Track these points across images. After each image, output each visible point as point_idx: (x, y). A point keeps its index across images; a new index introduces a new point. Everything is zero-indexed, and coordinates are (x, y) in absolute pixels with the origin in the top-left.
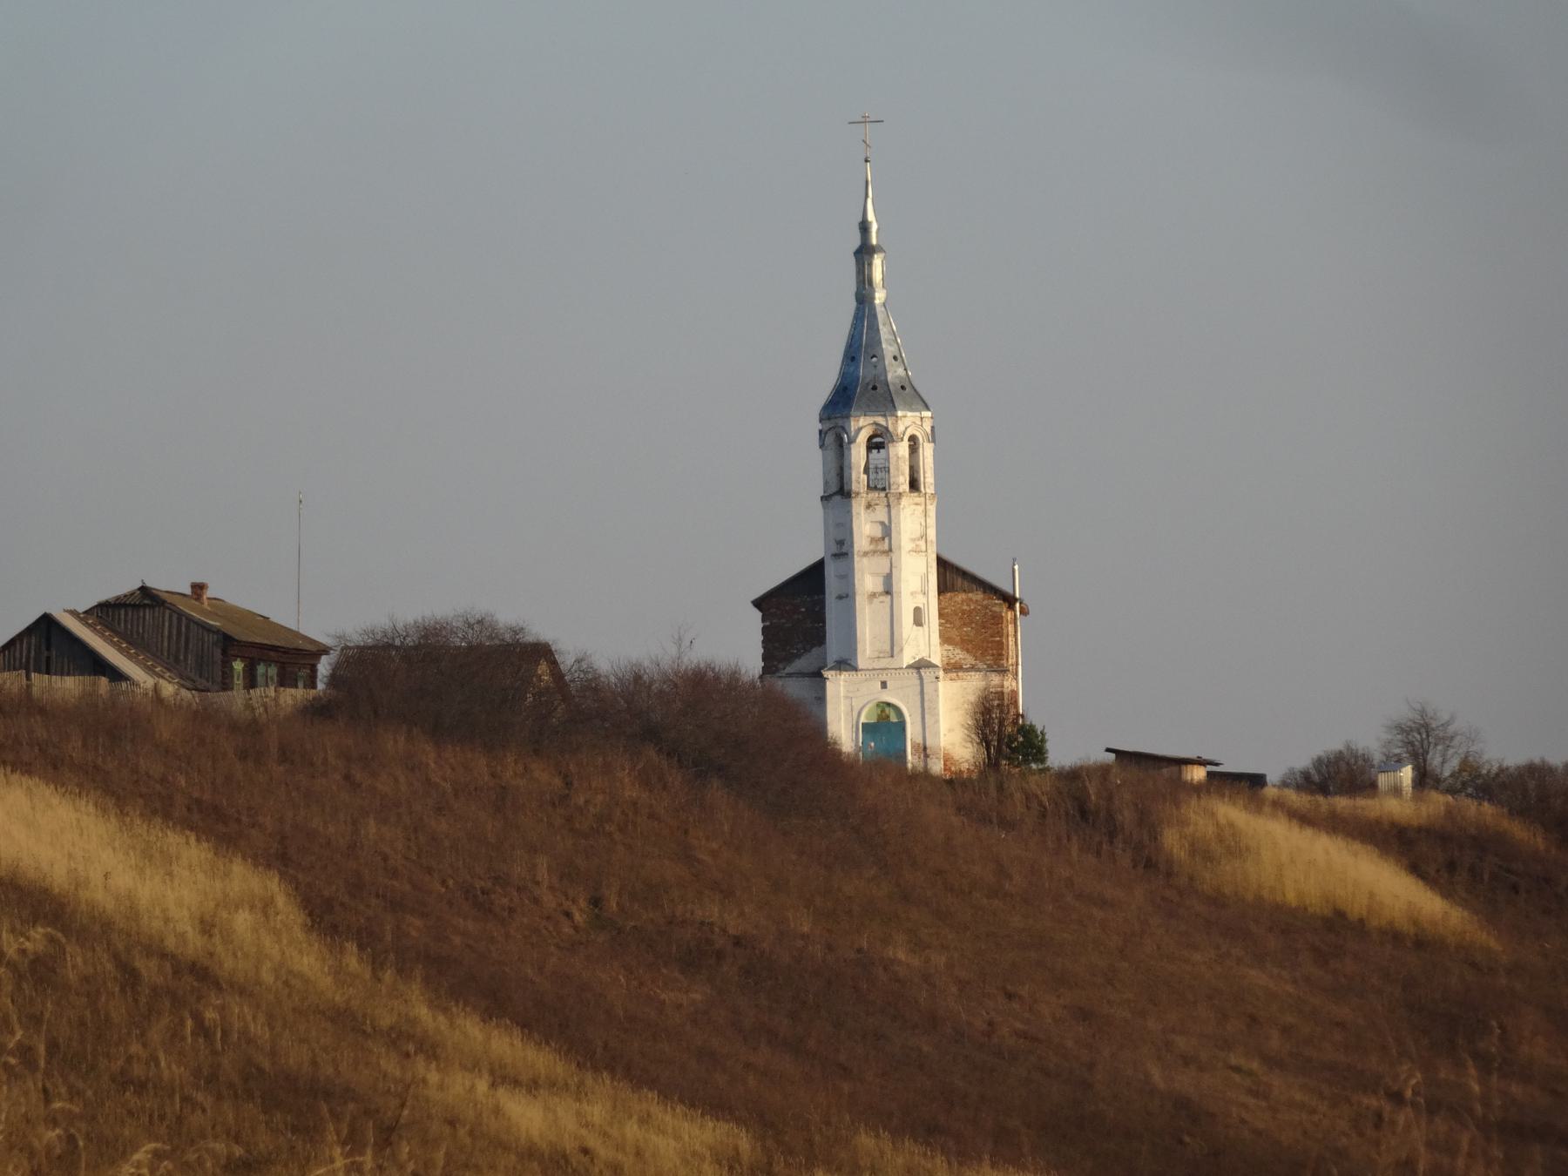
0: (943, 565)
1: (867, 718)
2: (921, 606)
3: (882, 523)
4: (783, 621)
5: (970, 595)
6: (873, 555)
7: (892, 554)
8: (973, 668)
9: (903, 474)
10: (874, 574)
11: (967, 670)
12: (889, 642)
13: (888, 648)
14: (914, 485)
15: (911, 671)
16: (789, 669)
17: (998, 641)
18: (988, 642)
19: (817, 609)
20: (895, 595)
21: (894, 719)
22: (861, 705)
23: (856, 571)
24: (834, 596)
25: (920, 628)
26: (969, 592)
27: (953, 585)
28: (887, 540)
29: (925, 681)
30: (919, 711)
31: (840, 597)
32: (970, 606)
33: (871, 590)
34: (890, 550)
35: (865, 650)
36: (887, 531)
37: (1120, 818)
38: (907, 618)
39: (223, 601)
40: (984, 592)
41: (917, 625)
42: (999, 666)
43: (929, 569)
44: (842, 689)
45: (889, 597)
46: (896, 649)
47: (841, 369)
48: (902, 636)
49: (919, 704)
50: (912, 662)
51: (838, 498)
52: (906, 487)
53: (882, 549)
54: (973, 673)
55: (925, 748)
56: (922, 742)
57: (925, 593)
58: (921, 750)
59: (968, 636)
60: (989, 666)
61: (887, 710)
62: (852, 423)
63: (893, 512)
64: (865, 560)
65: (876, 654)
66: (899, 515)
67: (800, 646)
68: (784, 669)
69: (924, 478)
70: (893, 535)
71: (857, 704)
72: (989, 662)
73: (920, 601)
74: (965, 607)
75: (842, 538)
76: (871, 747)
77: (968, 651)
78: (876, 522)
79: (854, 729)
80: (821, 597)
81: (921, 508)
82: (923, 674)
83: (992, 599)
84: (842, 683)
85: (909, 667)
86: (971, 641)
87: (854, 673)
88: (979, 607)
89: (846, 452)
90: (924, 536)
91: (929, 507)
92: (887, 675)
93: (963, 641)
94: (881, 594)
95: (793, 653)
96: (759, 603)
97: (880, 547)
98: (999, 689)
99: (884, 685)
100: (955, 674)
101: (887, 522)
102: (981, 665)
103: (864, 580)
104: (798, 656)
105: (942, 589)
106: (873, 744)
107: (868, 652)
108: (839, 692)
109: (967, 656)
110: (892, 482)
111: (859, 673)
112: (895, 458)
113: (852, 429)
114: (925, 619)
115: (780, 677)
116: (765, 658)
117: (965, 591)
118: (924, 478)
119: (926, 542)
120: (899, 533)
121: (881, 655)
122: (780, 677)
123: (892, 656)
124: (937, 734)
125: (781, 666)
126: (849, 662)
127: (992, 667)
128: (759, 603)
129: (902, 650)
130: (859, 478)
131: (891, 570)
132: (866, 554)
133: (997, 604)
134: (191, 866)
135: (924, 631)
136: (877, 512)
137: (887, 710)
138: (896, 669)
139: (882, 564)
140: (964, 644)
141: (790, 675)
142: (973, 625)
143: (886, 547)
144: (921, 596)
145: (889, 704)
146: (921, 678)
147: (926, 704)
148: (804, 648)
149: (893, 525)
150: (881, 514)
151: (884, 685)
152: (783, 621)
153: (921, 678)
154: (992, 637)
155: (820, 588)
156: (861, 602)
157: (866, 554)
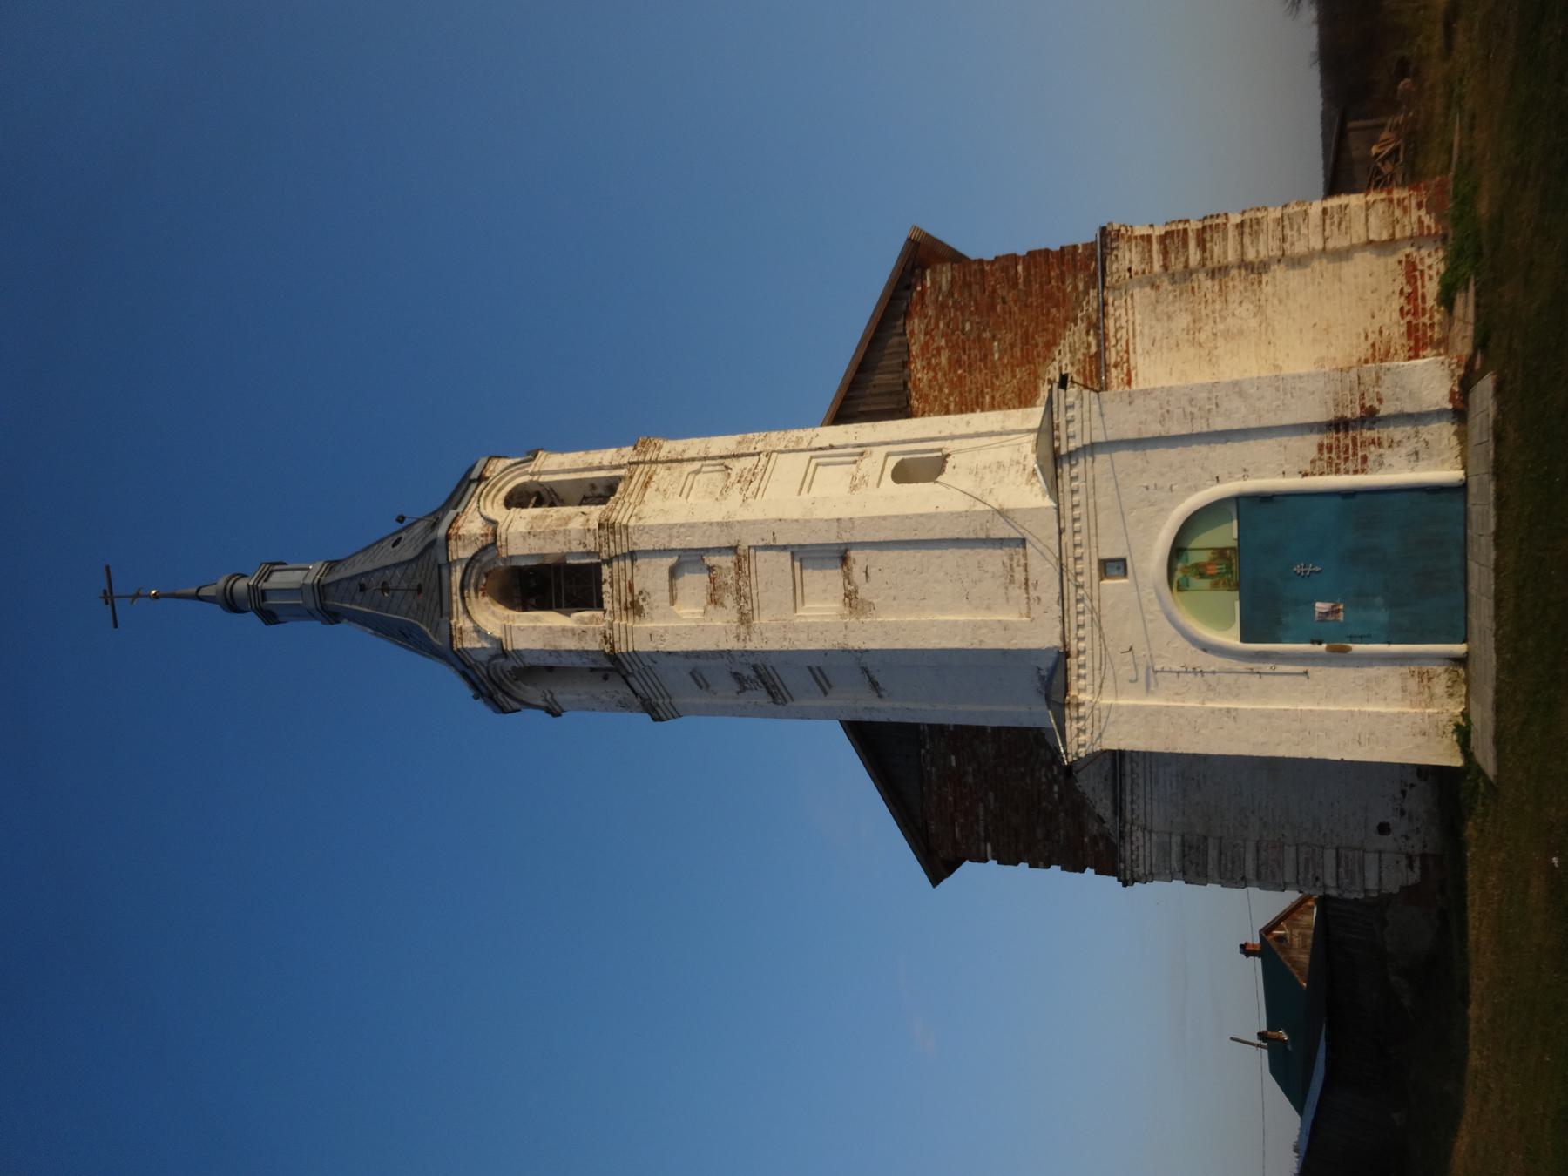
0: (842, 414)
1: (1224, 625)
2: (893, 462)
3: (674, 573)
4: (981, 812)
5: (915, 349)
7: (744, 546)
8: (1097, 326)
10: (797, 593)
11: (1103, 339)
12: (983, 553)
13: (998, 556)
14: (601, 492)
15: (1065, 484)
16: (1104, 807)
17: (1027, 269)
18: (1028, 293)
20: (846, 538)
21: (1226, 534)
22: (1180, 642)
23: (786, 646)
24: (878, 703)
26: (909, 351)
27: (891, 393)
28: (712, 560)
29: (1099, 437)
30: (1199, 451)
33: (838, 605)
34: (733, 549)
35: (1005, 626)
36: (687, 560)
37: (1122, 852)
38: (919, 498)
40: (907, 315)
41: (941, 471)
42: (1092, 257)
43: (804, 445)
44: (1124, 701)
45: (853, 554)
46: (1001, 530)
47: (424, 655)
48: (959, 515)
49: (1173, 454)
50: (1040, 484)
53: (733, 573)
54: (1111, 323)
55: (1339, 425)
56: (1315, 439)
57: (862, 450)
58: (1345, 440)
59: (1012, 346)
60: (1092, 282)
61: (1197, 557)
62: (467, 645)
63: (644, 543)
64: (762, 619)
65: (1017, 592)
66: (652, 527)
68: (1101, 820)
69: (600, 468)
70: (696, 542)
71: (1177, 654)
72: (1081, 286)
73: (877, 464)
74: (944, 360)
76: (1335, 611)
77: (1050, 345)
78: (672, 588)
79: (1266, 667)
80: (989, 731)
82: (1073, 445)
83: (922, 294)
84: (1106, 701)
85: (1054, 489)
86: (1027, 337)
87: (1072, 662)
89: (529, 661)
91: (663, 455)
92: (1080, 639)
93: (1027, 359)
94: (847, 576)
96: (938, 867)
97: (729, 578)
98: (1156, 247)
99: (1113, 567)
100: (1114, 372)
101: (672, 560)
102: (1090, 305)
103: (809, 626)
106: (1321, 607)
107: (1012, 617)
108: (1135, 710)
109: (1064, 345)
110: (581, 549)
111: (1074, 646)
112: (531, 540)
113: (478, 645)
116: (1074, 864)
117: (905, 364)
118: (600, 468)
120: (692, 526)
121: (1019, 575)
122: (1122, 836)
123: (1023, 542)
124: (1280, 383)
125: (1094, 828)
126: (1044, 673)
127: (1095, 274)
128: (938, 867)
129: (1002, 513)
130: (573, 631)
131: (784, 548)
132: (745, 619)
133: (933, 282)
134: (1195, 728)
135: (959, 451)
136: (649, 586)
137: (1197, 557)
138: (1061, 531)
139: (771, 570)
140: (1033, 352)
141: (1118, 807)
142: (987, 335)
143: (727, 561)
145: (1177, 550)
146: (1091, 449)
147: (1176, 429)
149: (675, 545)
150: (651, 576)
151: (1113, 567)
152: (981, 812)
153: (1091, 449)
154: (1016, 285)
155: (909, 733)
156: (868, 635)
157: (745, 619)
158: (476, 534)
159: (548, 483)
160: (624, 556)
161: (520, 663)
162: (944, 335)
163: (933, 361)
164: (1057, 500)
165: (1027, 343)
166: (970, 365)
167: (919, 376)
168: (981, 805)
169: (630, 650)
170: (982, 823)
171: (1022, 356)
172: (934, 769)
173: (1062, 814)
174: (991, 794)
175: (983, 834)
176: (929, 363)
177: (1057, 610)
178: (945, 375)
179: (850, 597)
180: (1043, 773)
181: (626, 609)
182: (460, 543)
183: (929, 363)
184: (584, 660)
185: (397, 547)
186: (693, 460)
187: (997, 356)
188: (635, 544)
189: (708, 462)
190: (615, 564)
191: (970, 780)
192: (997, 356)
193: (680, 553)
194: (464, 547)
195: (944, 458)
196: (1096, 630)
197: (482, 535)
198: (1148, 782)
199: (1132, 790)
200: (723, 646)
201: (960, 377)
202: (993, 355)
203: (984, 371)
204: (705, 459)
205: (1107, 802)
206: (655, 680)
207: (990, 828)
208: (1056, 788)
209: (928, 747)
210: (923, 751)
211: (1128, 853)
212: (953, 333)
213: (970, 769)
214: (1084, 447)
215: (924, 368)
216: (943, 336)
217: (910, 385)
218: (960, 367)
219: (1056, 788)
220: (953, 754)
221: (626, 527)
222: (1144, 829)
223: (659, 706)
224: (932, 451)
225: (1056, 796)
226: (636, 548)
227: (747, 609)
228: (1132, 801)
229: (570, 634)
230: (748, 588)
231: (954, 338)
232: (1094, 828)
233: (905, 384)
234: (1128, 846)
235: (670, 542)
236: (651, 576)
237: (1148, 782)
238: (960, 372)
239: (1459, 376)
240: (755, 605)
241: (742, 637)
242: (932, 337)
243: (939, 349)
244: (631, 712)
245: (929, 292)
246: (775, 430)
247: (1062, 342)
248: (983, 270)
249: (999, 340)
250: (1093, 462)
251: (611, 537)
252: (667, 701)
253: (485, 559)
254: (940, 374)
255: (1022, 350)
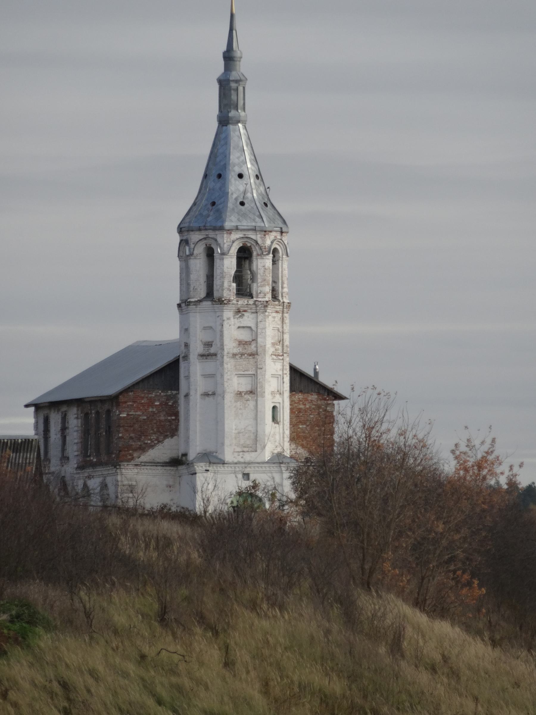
0: (294, 370)
2: (277, 405)
4: (139, 413)
6: (241, 358)
9: (268, 285)
16: (144, 458)
19: (170, 404)
24: (199, 393)
25: (277, 425)
31: (206, 395)
32: (305, 405)
39: (146, 341)
40: (318, 393)
48: (264, 432)
51: (207, 304)
52: (269, 297)
59: (304, 432)
67: (154, 437)
74: (302, 406)
75: (210, 340)
81: (280, 315)
86: (305, 438)
88: (313, 406)
90: (281, 341)
95: (147, 443)
101: (254, 328)
104: (152, 447)
105: (292, 389)
110: (259, 291)
114: (280, 417)
115: (136, 465)
119: (283, 346)
122: (136, 465)
125: (135, 455)
136: (245, 318)
144: (278, 396)
148: (157, 439)
152: (139, 413)
158: (266, 243)
159: (279, 264)
160: (256, 310)
161: (233, 308)
162: (310, 407)
163: (301, 403)
164: (267, 463)
165: (304, 438)
166: (298, 416)
167: (297, 397)
168: (141, 414)
169: (224, 310)
170: (134, 413)
171: (300, 436)
172: (153, 396)
173: (140, 444)
174: (145, 417)
175: (130, 413)
176: (300, 401)
177: (236, 461)
178: (296, 407)
179: (240, 394)
180: (155, 437)
181: (238, 309)
182: (263, 236)
183: (300, 401)
184: (218, 287)
185: (263, 204)
186: (283, 328)
187: (301, 426)
188: (260, 315)
189: (282, 334)
190: (254, 306)
191: (151, 410)
192: (301, 426)
193: (256, 331)
194: (261, 238)
195: (278, 423)
196: (230, 472)
197: (265, 247)
198: (153, 474)
199: (151, 469)
200: (225, 348)
201: (295, 413)
202: (301, 425)
203: (296, 422)
204: (283, 333)
205: (145, 460)
206: (207, 311)
207: (132, 416)
208: (149, 442)
209: (162, 394)
210: (160, 392)
211: (130, 467)
212: (310, 411)
213: (154, 410)
214: (282, 471)
215: (299, 399)
216: (310, 407)
217: (294, 392)
218: (298, 413)
219: (149, 442)
220: (160, 404)
221: (266, 311)
222: (138, 473)
223: (196, 307)
224: (280, 418)
225: (146, 442)
226: (258, 315)
227: (237, 357)
228: (147, 469)
229: (229, 285)
230: (244, 358)
231: (309, 411)
232: (135, 455)
233: (294, 391)
234: (132, 467)
235: (260, 329)
236: (248, 320)
237: (153, 474)
238: (296, 412)
239: (334, 388)
240: (238, 360)
241: (228, 355)
242: (310, 403)
243: (305, 405)
244: (264, 392)
245: (326, 402)
246: (231, 96)
247: (303, 450)
248: (330, 423)
249: (306, 428)
250: (143, 486)
251: (263, 306)
252: (198, 311)
253: (257, 248)
254: (296, 405)
255: (302, 436)
